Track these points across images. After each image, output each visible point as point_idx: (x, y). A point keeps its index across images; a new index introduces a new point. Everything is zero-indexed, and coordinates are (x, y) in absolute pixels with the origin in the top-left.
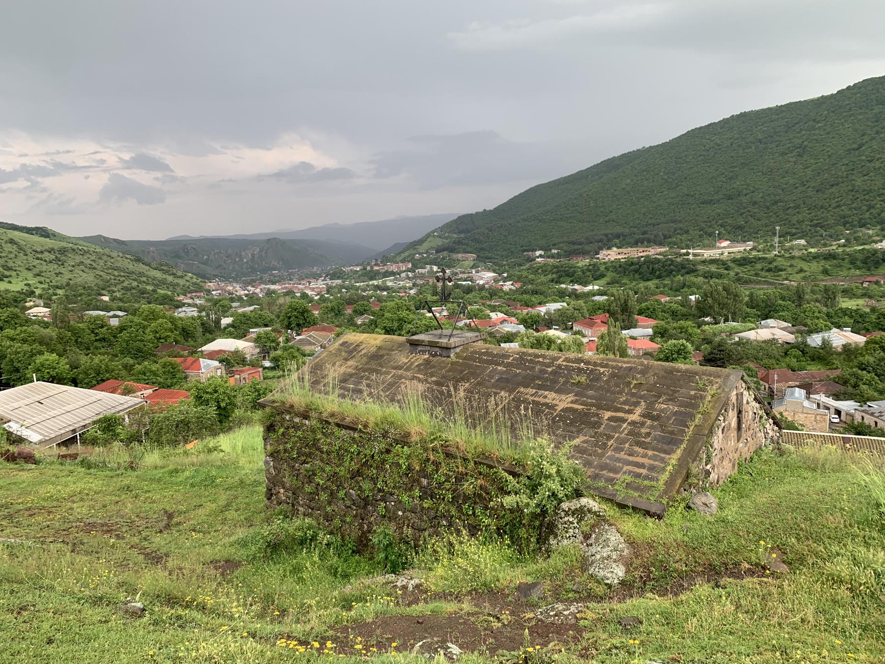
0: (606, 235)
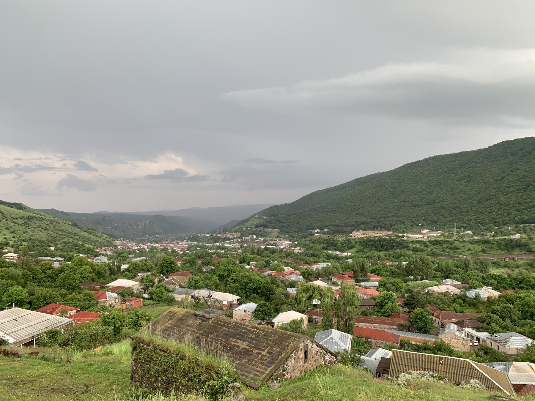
0: (357, 222)
